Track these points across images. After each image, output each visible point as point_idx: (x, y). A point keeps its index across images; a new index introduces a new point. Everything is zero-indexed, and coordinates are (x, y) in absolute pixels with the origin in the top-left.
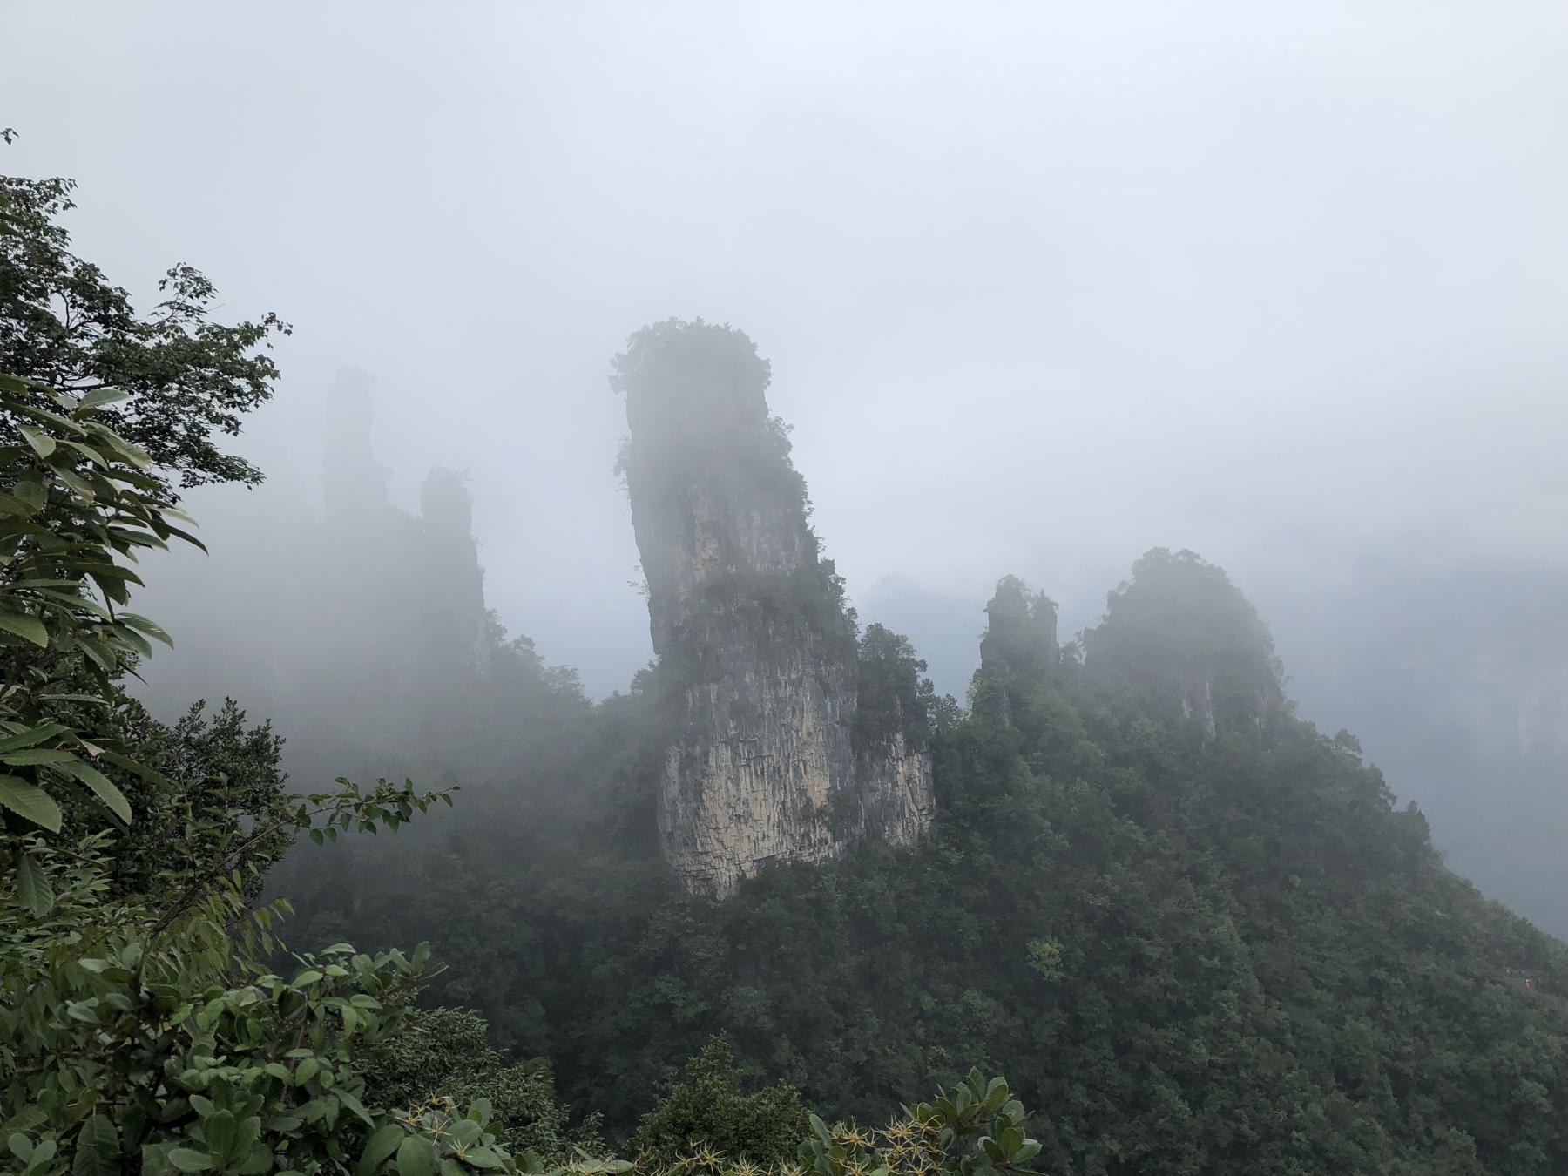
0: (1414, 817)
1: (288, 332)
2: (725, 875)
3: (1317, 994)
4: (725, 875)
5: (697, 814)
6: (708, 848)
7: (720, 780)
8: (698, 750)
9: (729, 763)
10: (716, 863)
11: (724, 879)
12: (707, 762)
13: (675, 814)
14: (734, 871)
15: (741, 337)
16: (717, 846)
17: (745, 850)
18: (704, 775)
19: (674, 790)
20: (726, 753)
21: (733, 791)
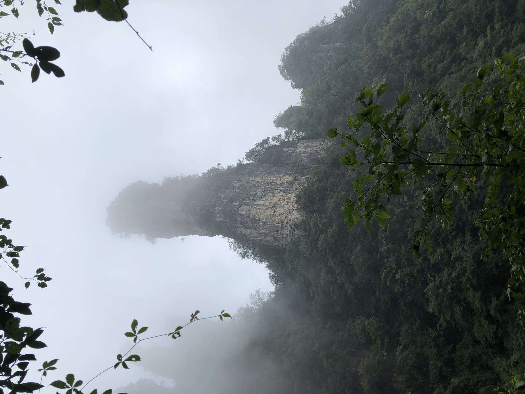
0: (132, 184)
1: (22, 4)
2: (296, 216)
3: (304, 150)
4: (296, 216)
5: (264, 223)
6: (280, 221)
7: (254, 211)
8: (239, 218)
9: (249, 207)
10: (288, 218)
11: (297, 216)
12: (244, 215)
13: (266, 235)
14: (295, 212)
15: (139, 181)
16: (281, 216)
17: (289, 206)
18: (249, 217)
19: (255, 232)
20: (245, 207)
21: (261, 207)
